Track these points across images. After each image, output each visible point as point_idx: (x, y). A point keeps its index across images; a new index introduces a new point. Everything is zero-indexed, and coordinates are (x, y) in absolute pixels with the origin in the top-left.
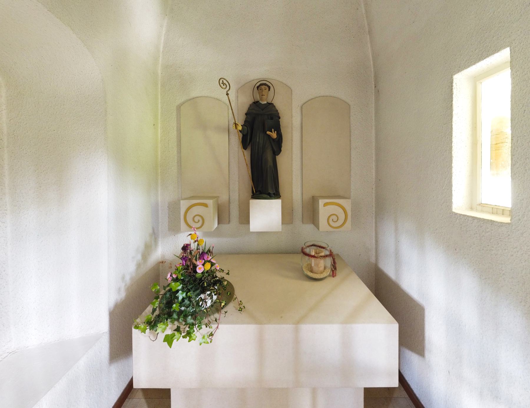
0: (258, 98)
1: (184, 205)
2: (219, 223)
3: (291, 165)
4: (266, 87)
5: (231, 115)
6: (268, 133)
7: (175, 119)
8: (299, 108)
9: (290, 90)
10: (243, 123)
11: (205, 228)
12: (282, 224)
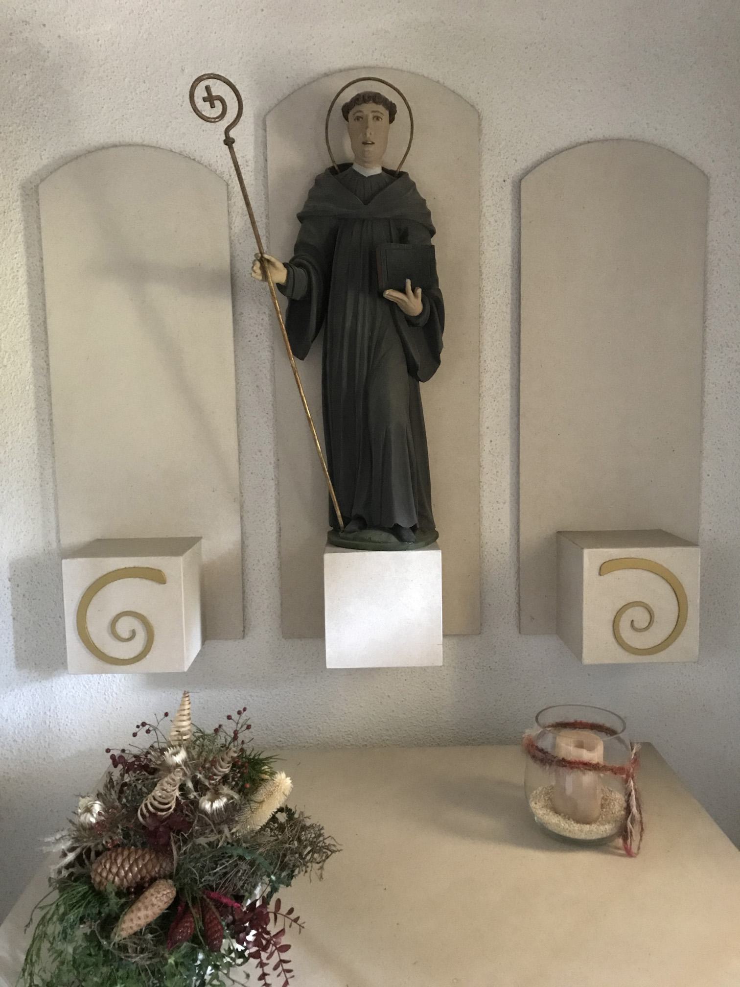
0: (347, 150)
1: (76, 575)
2: (206, 636)
3: (476, 419)
4: (381, 108)
5: (240, 221)
6: (391, 294)
7: (20, 238)
8: (508, 188)
9: (470, 116)
10: (289, 255)
11: (155, 662)
12: (445, 636)
